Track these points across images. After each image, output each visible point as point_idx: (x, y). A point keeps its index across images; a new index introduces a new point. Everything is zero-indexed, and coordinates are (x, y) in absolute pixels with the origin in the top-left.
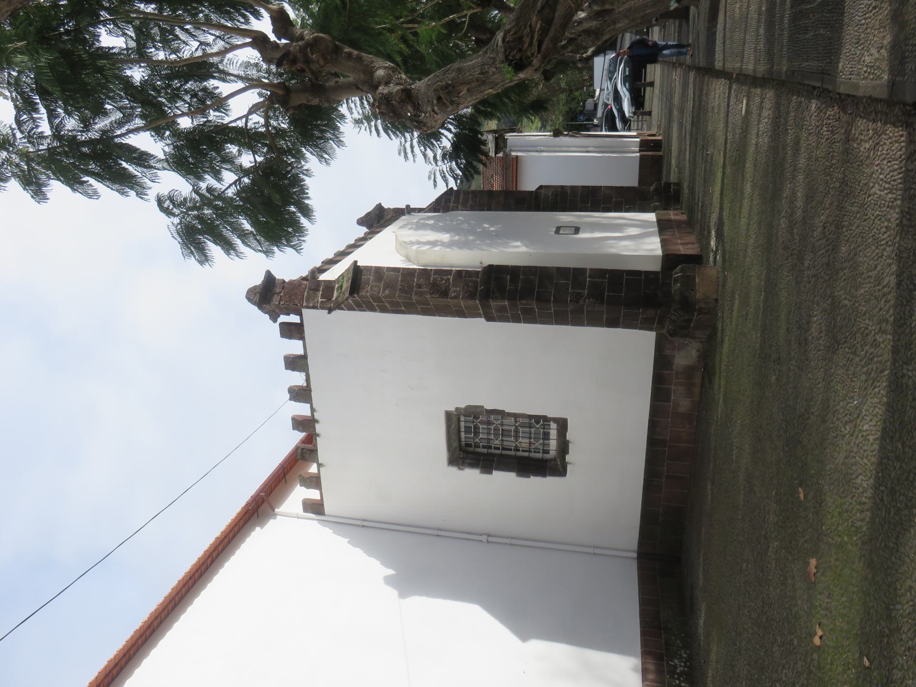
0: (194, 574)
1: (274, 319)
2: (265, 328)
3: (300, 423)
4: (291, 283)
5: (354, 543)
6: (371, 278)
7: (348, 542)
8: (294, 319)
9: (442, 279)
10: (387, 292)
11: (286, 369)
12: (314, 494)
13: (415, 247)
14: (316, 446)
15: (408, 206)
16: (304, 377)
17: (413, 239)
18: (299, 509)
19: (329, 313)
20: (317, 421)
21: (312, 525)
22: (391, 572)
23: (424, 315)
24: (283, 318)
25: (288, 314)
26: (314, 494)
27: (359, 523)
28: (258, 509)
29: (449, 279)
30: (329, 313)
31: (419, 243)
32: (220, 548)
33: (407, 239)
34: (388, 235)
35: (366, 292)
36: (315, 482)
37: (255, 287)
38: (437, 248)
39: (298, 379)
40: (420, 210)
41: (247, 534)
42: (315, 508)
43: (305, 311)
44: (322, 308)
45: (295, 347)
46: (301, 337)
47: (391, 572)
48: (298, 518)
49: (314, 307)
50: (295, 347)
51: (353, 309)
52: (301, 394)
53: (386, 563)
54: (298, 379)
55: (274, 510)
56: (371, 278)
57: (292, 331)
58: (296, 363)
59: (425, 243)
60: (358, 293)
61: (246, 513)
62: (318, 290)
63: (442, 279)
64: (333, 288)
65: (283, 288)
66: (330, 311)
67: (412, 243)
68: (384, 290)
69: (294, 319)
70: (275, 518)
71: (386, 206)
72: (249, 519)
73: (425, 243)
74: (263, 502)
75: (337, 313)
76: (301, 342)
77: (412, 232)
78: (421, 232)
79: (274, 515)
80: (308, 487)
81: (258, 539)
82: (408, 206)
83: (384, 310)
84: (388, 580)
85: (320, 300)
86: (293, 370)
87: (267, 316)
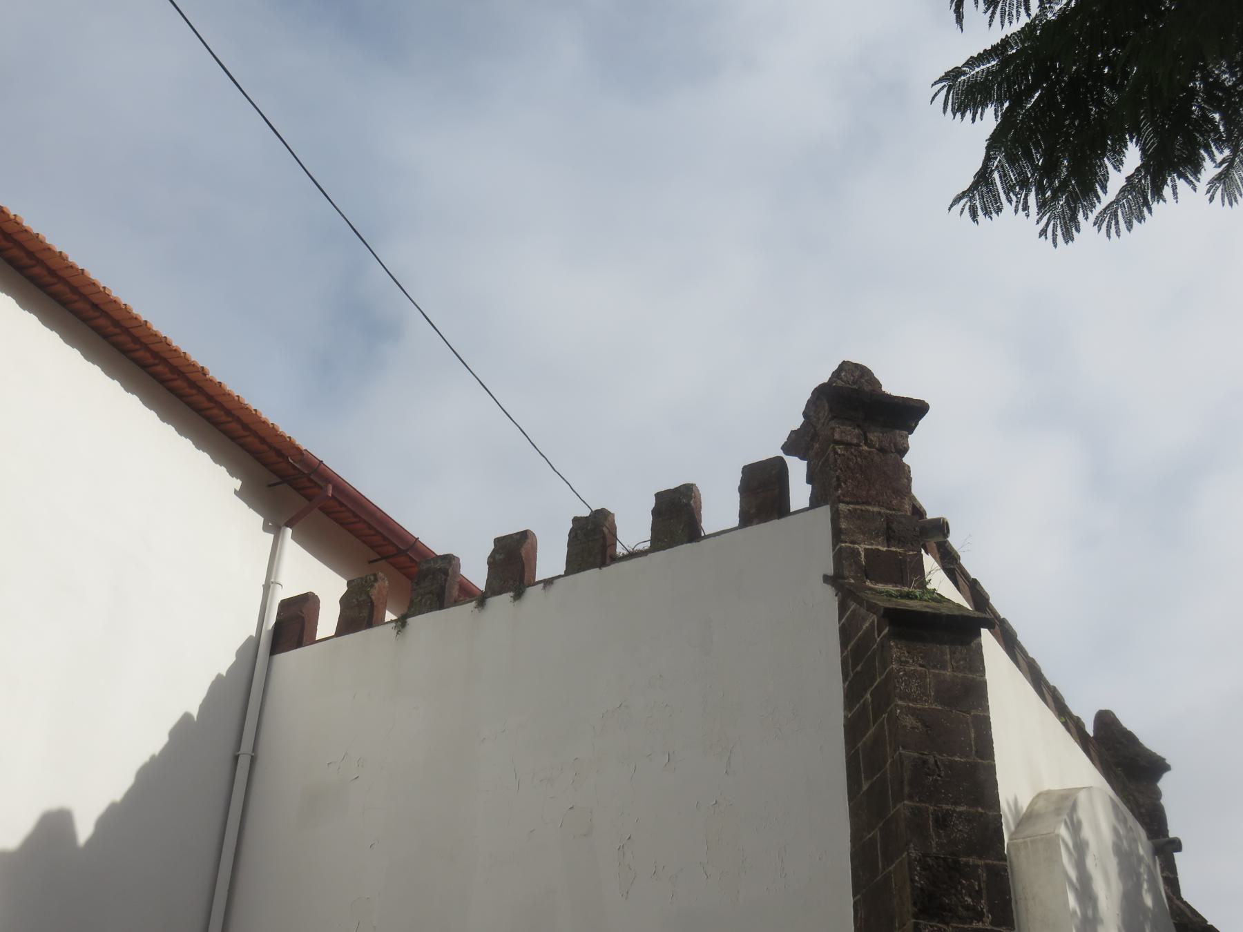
0: (106, 315)
1: (795, 444)
2: (770, 418)
3: (512, 560)
4: (903, 474)
5: (184, 731)
6: (948, 673)
7: (187, 717)
8: (800, 492)
9: (977, 895)
10: (909, 721)
11: (659, 496)
12: (327, 622)
13: (1063, 832)
14: (456, 603)
15: (1176, 845)
16: (640, 547)
17: (1087, 833)
18: (288, 589)
19: (826, 579)
20: (518, 595)
21: (241, 620)
22: (84, 830)
23: (845, 726)
24: (797, 469)
25: (810, 480)
26: (327, 622)
27: (246, 747)
28: (289, 484)
29: (980, 916)
30: (826, 579)
31: (1080, 849)
32: (179, 383)
33: (1082, 814)
34: (1081, 773)
35: (901, 659)
36: (358, 614)
37: (877, 384)
38: (1072, 902)
39: (633, 530)
40: (1172, 882)
41: (219, 456)
42: (292, 624)
43: (825, 512)
44: (839, 557)
45: (720, 509)
46: (747, 518)
47: (84, 830)
48: (267, 587)
49: (837, 534)
50: (720, 509)
51: (844, 644)
52: (592, 541)
53: (113, 819)
54: (633, 530)
55: (288, 525)
56: (948, 673)
57: (762, 491)
58: (676, 515)
59: (1080, 865)
60: (893, 635)
61: (279, 453)
62: (889, 541)
63: (977, 895)
64: (901, 581)
65: (882, 450)
66: (833, 580)
67: (1075, 828)
68: (914, 712)
69: (800, 492)
70: (266, 528)
71: (1165, 784)
72: (265, 464)
73: (1080, 865)
74: (309, 498)
75: (828, 599)
76: (735, 522)
77: (1108, 836)
78: (1113, 864)
79: (274, 525)
80: (345, 601)
81: (206, 486)
82: (1176, 845)
83: (853, 730)
84: (55, 825)
85: (861, 548)
86: (656, 513)
87: (797, 422)
